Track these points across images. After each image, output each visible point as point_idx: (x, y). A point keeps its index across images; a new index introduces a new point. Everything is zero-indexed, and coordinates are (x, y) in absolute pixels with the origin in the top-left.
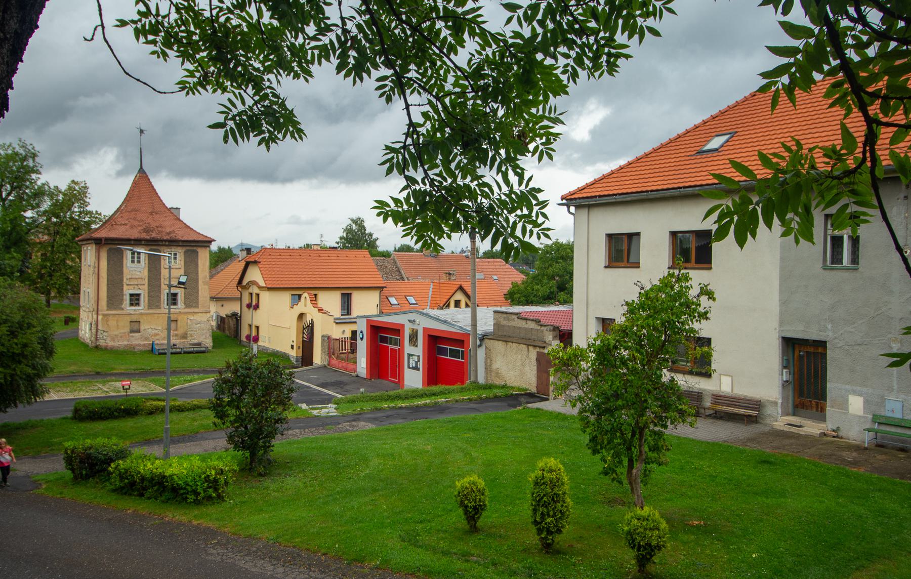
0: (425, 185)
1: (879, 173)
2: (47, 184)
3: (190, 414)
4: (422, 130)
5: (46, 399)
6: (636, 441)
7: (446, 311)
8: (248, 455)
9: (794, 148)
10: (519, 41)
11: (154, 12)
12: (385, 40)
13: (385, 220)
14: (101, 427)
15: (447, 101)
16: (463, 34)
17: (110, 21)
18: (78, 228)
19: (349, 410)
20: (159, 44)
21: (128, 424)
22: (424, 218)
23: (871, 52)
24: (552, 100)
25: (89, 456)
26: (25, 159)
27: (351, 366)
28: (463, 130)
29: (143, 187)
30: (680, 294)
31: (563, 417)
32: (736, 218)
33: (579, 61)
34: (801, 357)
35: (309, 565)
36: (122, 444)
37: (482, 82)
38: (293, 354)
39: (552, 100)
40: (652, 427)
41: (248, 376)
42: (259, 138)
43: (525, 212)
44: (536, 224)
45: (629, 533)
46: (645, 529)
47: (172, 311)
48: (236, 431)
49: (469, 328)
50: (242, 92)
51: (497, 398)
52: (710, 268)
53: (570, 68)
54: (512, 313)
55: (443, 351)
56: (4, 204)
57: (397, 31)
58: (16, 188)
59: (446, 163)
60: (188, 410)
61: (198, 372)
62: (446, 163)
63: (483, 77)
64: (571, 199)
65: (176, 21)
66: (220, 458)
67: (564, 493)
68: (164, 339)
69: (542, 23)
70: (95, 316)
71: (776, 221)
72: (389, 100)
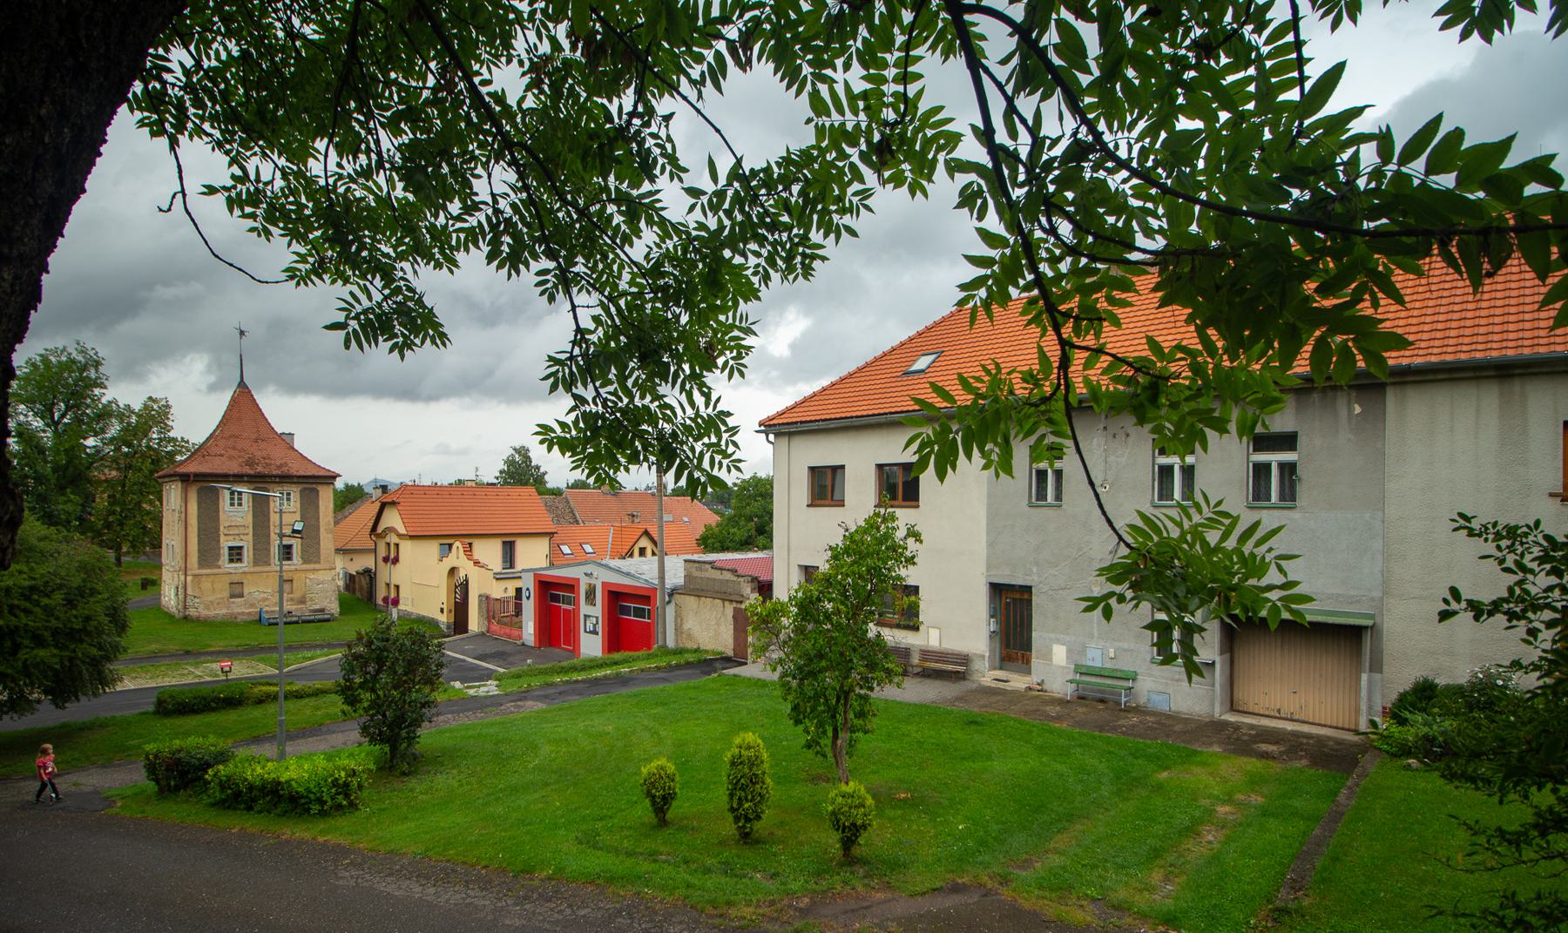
0: (596, 405)
1: (1073, 400)
2: (115, 401)
3: (312, 701)
4: (593, 338)
5: (119, 688)
6: (841, 708)
7: (629, 561)
8: (387, 749)
9: (994, 372)
10: (703, 234)
11: (253, 177)
12: (546, 224)
13: (549, 450)
14: (194, 722)
15: (622, 302)
16: (639, 222)
17: (193, 186)
18: (158, 461)
19: (513, 687)
20: (260, 219)
21: (230, 717)
22: (596, 447)
23: (1064, 267)
24: (743, 307)
25: (178, 762)
26: (85, 368)
27: (515, 632)
28: (640, 340)
29: (243, 406)
30: (887, 536)
31: (760, 684)
32: (936, 448)
33: (771, 261)
34: (1008, 604)
35: (466, 881)
36: (222, 744)
37: (662, 282)
38: (443, 619)
39: (743, 307)
40: (857, 690)
41: (386, 650)
42: (390, 343)
43: (714, 439)
44: (726, 455)
45: (833, 813)
46: (850, 807)
47: (285, 568)
48: (372, 720)
49: (656, 582)
50: (368, 284)
51: (689, 665)
52: (918, 507)
53: (761, 269)
54: (704, 562)
55: (626, 610)
56: (56, 428)
57: (560, 215)
58: (72, 407)
59: (622, 379)
60: (309, 695)
61: (321, 647)
62: (622, 379)
63: (663, 275)
64: (770, 426)
65: (282, 189)
66: (351, 755)
67: (764, 773)
68: (275, 605)
69: (729, 213)
70: (182, 578)
71: (976, 452)
72: (552, 299)
